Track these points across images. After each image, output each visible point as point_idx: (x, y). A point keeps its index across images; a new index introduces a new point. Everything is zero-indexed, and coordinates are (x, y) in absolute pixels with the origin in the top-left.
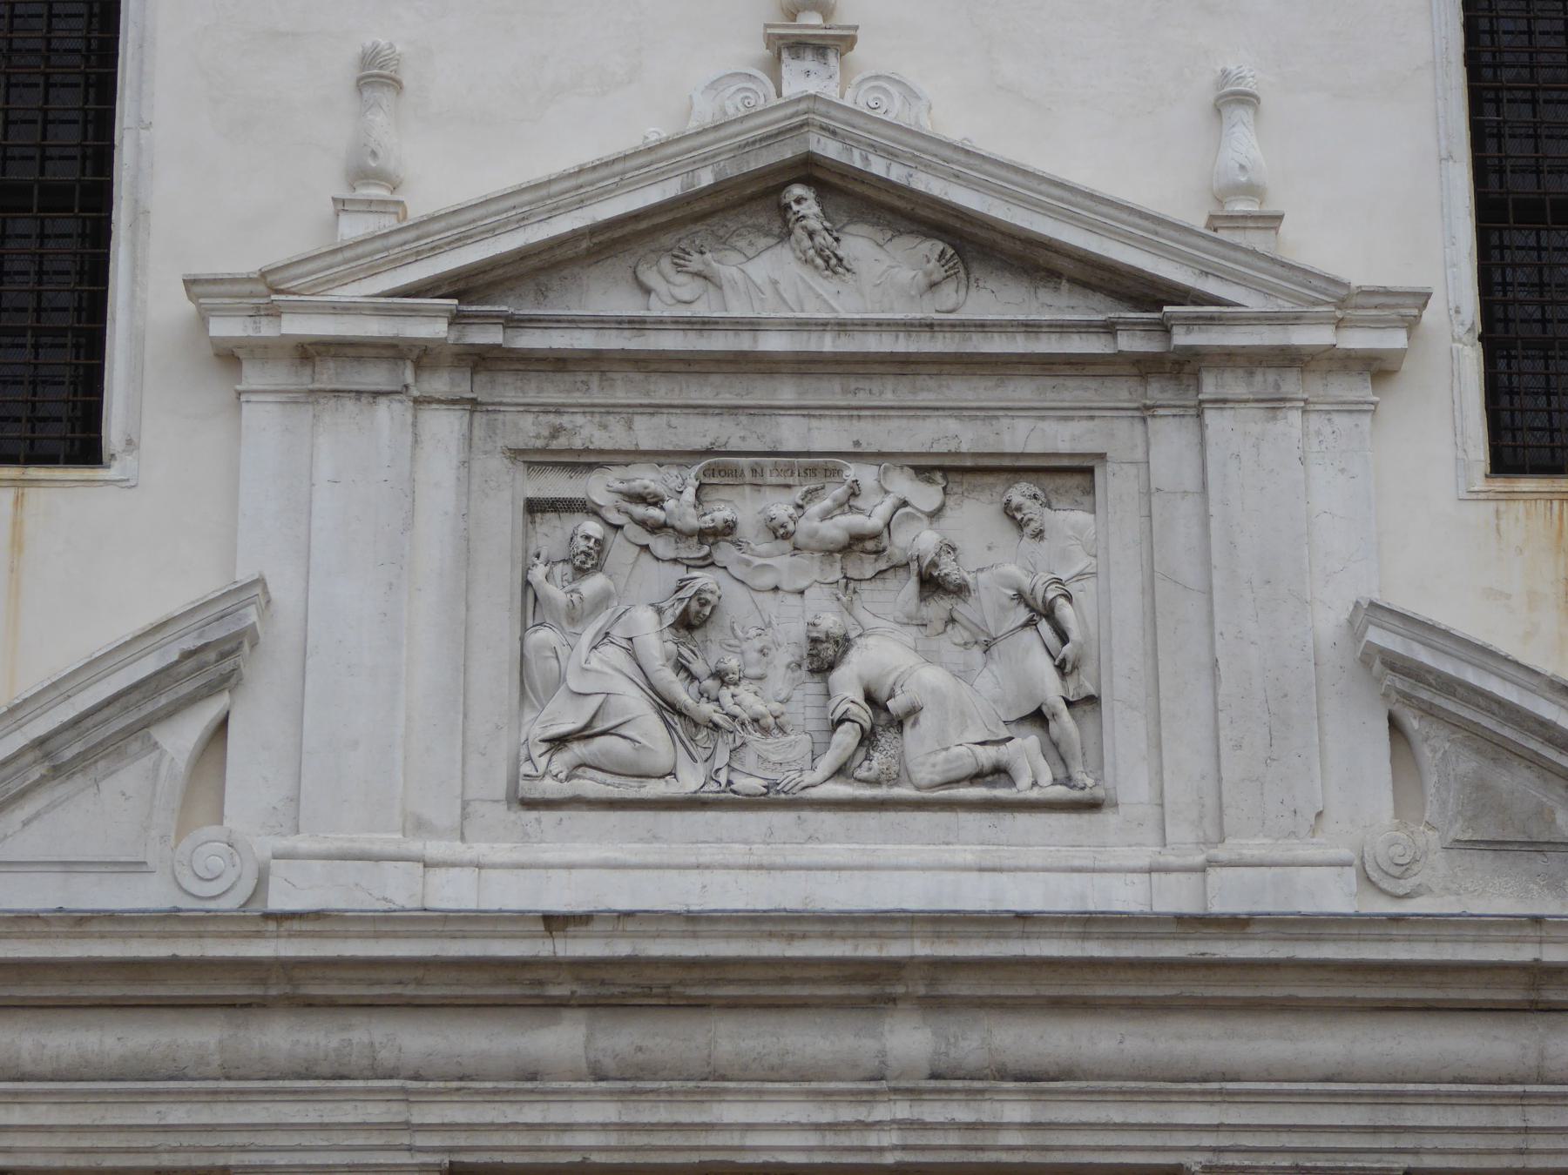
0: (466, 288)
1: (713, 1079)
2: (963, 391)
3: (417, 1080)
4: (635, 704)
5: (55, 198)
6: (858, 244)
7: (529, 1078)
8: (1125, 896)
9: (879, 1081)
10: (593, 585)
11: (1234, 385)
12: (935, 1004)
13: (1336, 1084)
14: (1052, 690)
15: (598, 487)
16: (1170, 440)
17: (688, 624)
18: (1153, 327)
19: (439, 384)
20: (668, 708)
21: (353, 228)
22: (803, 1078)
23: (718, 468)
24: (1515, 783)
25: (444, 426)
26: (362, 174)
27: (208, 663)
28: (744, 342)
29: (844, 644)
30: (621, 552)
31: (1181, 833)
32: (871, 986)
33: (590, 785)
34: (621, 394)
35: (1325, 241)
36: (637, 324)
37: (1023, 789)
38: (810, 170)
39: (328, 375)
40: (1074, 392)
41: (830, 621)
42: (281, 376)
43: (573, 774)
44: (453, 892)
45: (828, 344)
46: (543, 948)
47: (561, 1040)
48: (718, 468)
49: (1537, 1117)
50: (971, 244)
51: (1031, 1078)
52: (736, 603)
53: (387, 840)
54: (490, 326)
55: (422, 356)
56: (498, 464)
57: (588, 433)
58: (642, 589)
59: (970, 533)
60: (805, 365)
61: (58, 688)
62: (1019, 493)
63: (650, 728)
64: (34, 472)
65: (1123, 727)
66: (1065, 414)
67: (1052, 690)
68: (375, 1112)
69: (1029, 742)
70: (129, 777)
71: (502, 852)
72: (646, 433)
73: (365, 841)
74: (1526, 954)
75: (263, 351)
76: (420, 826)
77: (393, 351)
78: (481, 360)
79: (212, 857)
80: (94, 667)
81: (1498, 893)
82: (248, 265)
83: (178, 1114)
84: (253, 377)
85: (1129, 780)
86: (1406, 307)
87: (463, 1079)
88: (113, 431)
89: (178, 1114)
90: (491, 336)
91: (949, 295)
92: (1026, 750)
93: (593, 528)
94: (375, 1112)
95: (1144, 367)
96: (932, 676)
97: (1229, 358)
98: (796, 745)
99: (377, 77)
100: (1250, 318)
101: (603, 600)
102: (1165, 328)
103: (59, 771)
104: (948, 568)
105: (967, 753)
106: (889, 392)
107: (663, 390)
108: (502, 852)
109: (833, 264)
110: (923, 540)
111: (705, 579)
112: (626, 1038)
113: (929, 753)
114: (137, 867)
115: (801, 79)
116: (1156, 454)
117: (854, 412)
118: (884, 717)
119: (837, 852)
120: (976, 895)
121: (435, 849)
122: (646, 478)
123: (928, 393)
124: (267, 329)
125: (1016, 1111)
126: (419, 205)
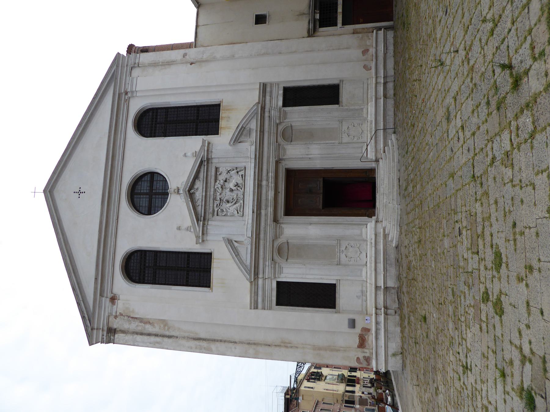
0: (198, 221)
1: (267, 199)
2: (209, 178)
3: (266, 224)
4: (235, 206)
6: (196, 187)
7: (266, 215)
8: (253, 165)
9: (267, 185)
10: (224, 210)
12: (261, 181)
13: (269, 148)
14: (235, 171)
15: (216, 210)
16: (214, 161)
17: (228, 202)
18: (204, 162)
19: (206, 223)
20: (235, 203)
21: (192, 230)
23: (215, 199)
24: (244, 133)
25: (210, 223)
27: (230, 242)
30: (222, 208)
33: (242, 210)
34: (208, 207)
35: (197, 147)
36: (202, 206)
37: (244, 174)
38: (189, 191)
39: (205, 232)
40: (210, 169)
41: (229, 190)
42: (205, 236)
43: (241, 212)
44: (250, 221)
45: (204, 189)
47: (263, 212)
48: (215, 199)
50: (196, 177)
52: (227, 198)
53: (246, 227)
54: (201, 218)
55: (204, 224)
56: (213, 218)
57: (211, 210)
58: (225, 206)
59: (221, 178)
60: (206, 192)
61: (231, 254)
62: (218, 174)
63: (237, 205)
65: (239, 165)
66: (211, 169)
67: (235, 171)
68: (268, 228)
69: (239, 173)
70: (239, 249)
71: (247, 217)
72: (211, 205)
75: (202, 238)
76: (245, 224)
77: (203, 227)
78: (204, 219)
79: (246, 242)
80: (230, 252)
81: (254, 134)
82: (195, 239)
83: (268, 244)
84: (205, 239)
85: (243, 164)
86: (204, 141)
87: (266, 220)
88: (209, 251)
89: (268, 244)
90: (202, 218)
91: (201, 179)
92: (240, 173)
94: (268, 228)
95: (208, 163)
96: (234, 181)
97: (207, 155)
99: (179, 228)
103: (238, 255)
104: (224, 179)
105: (240, 178)
106: (209, 185)
107: (208, 204)
108: (247, 217)
109: (197, 189)
112: (263, 207)
113: (240, 181)
114: (247, 248)
115: (181, 192)
116: (215, 162)
118: (237, 185)
119: (248, 189)
120: (251, 207)
122: (215, 205)
123: (209, 181)
125: (270, 174)
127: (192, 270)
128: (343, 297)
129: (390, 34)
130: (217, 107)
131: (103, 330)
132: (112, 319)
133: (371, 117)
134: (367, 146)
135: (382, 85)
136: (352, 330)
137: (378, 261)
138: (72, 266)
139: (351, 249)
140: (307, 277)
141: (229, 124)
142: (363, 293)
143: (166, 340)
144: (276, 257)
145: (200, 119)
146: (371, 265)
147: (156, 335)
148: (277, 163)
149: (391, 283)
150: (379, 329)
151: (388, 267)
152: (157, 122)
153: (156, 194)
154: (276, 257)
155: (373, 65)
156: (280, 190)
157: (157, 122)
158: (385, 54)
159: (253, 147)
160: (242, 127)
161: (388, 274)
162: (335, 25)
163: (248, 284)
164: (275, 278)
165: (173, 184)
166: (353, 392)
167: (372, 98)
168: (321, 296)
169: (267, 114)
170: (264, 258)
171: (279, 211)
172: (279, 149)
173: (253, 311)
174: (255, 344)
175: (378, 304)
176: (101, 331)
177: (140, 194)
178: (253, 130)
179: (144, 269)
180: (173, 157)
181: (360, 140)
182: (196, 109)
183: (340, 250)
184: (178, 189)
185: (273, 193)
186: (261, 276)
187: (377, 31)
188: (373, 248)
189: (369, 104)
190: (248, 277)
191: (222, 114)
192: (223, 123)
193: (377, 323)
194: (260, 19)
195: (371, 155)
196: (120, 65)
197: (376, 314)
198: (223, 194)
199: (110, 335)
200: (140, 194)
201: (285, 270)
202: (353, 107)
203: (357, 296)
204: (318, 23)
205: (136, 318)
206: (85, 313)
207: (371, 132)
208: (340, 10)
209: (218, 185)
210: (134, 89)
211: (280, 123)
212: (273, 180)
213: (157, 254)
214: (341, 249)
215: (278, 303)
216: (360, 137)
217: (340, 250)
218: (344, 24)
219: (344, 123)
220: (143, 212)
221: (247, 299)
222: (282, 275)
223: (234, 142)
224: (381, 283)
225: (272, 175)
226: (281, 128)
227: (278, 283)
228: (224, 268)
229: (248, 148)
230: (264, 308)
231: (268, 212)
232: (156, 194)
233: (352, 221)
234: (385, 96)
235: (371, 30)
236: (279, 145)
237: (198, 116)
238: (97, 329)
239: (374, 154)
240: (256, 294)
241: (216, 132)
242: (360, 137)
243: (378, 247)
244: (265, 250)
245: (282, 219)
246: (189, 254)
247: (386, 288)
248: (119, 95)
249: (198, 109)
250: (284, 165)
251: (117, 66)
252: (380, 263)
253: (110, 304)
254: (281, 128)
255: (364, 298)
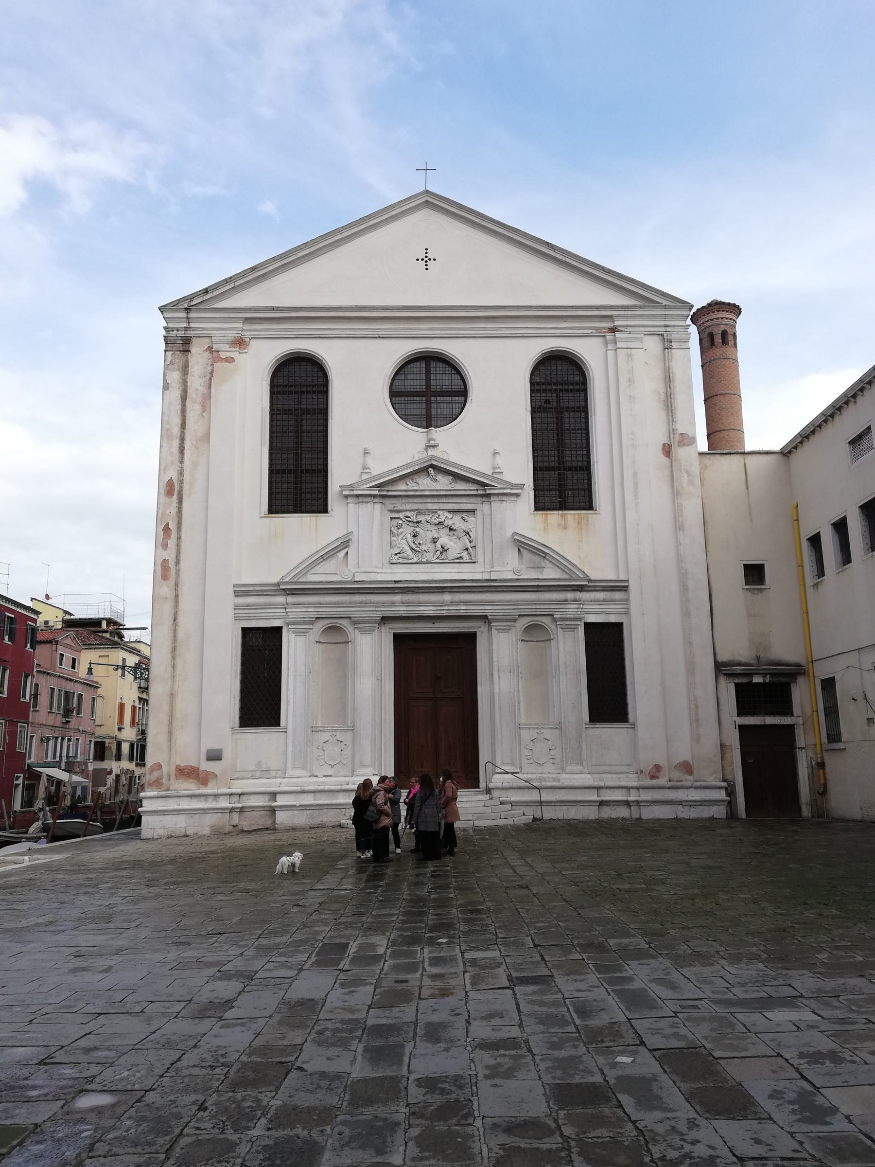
0: (380, 486)
1: (419, 604)
3: (377, 604)
4: (407, 548)
5: (320, 471)
6: (440, 477)
7: (393, 604)
8: (479, 577)
9: (443, 604)
10: (401, 530)
11: (496, 498)
15: (401, 515)
16: (486, 506)
17: (414, 536)
18: (484, 490)
19: (377, 500)
20: (412, 549)
21: (364, 477)
22: (433, 603)
23: (419, 512)
24: (536, 559)
25: (378, 506)
26: (365, 468)
27: (345, 544)
28: (422, 493)
29: (438, 539)
30: (404, 525)
31: (487, 566)
32: (442, 590)
33: (401, 561)
35: (509, 477)
38: (432, 466)
40: (472, 500)
41: (436, 536)
43: (399, 559)
44: (381, 578)
45: (435, 493)
46: (394, 586)
47: (398, 598)
48: (419, 512)
49: (538, 607)
51: (465, 603)
54: (384, 492)
55: (375, 496)
57: (399, 507)
58: (408, 530)
59: (456, 521)
62: (464, 515)
63: (409, 552)
64: (549, 512)
65: (480, 551)
66: (471, 503)
67: (469, 545)
68: (371, 609)
69: (465, 553)
72: (408, 507)
73: (368, 570)
74: (536, 584)
79: (347, 573)
82: (348, 484)
84: (350, 500)
85: (480, 559)
86: (521, 486)
87: (384, 604)
88: (329, 509)
89: (343, 609)
90: (385, 493)
93: (400, 522)
94: (371, 609)
95: (482, 496)
96: (451, 543)
97: (495, 494)
98: (430, 555)
99: (366, 453)
100: (498, 488)
101: (402, 533)
102: (485, 490)
104: (453, 527)
106: (444, 500)
107: (410, 500)
108: (388, 571)
109: (436, 481)
110: (450, 523)
111: (417, 529)
113: (453, 554)
115: (431, 452)
116: (483, 508)
117: (439, 503)
118: (444, 550)
121: (378, 571)
124: (351, 493)
126: (374, 473)
127: (298, 478)
128: (260, 739)
129: (719, 812)
130: (589, 505)
131: (186, 329)
132: (206, 342)
133: (566, 779)
134: (512, 773)
135: (625, 798)
136: (203, 756)
137: (318, 795)
138: (293, 261)
139: (337, 749)
140: (291, 679)
141: (556, 531)
142: (266, 773)
143: (176, 443)
144: (322, 624)
145: (564, 475)
146: (311, 784)
147: (183, 425)
148: (484, 618)
149: (282, 818)
150: (206, 801)
151: (308, 812)
152: (560, 394)
153: (428, 403)
154: (322, 624)
155: (662, 781)
156: (437, 625)
157: (560, 394)
158: (680, 803)
159: (510, 576)
160: (546, 554)
161: (296, 812)
162: (740, 713)
163: (275, 580)
164: (288, 624)
165: (440, 434)
166: (118, 757)
167: (601, 780)
168: (260, 704)
169: (570, 595)
170: (319, 604)
171: (401, 625)
172: (507, 620)
173: (231, 590)
174: (177, 596)
175: (247, 797)
176: (185, 325)
177: (428, 373)
178: (542, 573)
179: (296, 393)
180: (495, 433)
181: (524, 761)
182: (585, 464)
183: (336, 731)
184: (433, 446)
185: (431, 613)
186: (291, 599)
187: (726, 789)
188: (338, 787)
189: (589, 776)
190: (287, 580)
191: (571, 516)
192: (554, 516)
193: (216, 796)
194: (754, 574)
195: (498, 780)
196: (667, 313)
197: (231, 795)
198: (429, 526)
199: (179, 344)
200: (428, 373)
201: (301, 640)
202: (584, 747)
203: (260, 762)
204: (744, 680)
205: (210, 387)
206: (215, 293)
207: (540, 780)
208: (770, 720)
209: (443, 516)
210: (619, 345)
211: (555, 620)
212: (453, 613)
213: (323, 413)
214: (338, 733)
215: (245, 631)
216: (531, 761)
217: (336, 731)
218: (742, 729)
219: (557, 731)
220: (396, 383)
221: (248, 579)
222: (292, 636)
223: (518, 541)
224: (281, 801)
225: (462, 610)
226: (546, 621)
227: (279, 630)
228: (304, 533)
229: (511, 567)
230: (236, 607)
231: (398, 605)
232: (428, 403)
233: (385, 750)
234: (602, 803)
235: (729, 777)
236: (515, 620)
237: (570, 469)
238: (188, 318)
239: (499, 785)
240: (260, 593)
241: (539, 506)
242: (531, 761)
243: (341, 794)
244: (336, 604)
245: (387, 630)
246: (323, 472)
247: (273, 811)
248: (611, 317)
249: (585, 469)
250: (482, 629)
251: (665, 307)
252: (315, 799)
253: (230, 339)
254: (546, 621)
255: (258, 774)
